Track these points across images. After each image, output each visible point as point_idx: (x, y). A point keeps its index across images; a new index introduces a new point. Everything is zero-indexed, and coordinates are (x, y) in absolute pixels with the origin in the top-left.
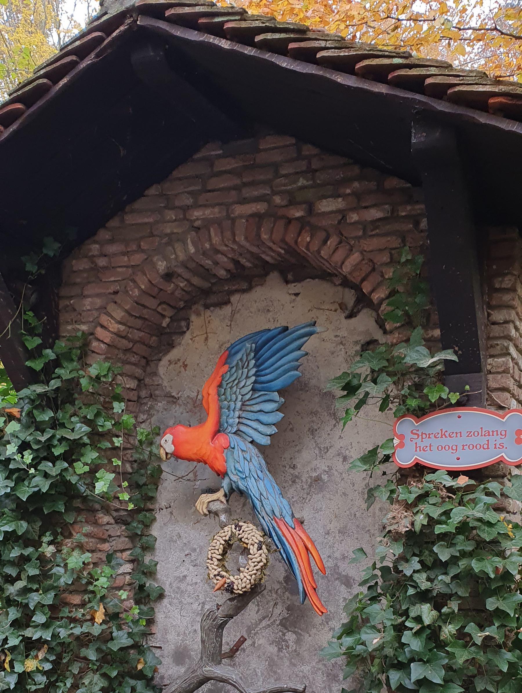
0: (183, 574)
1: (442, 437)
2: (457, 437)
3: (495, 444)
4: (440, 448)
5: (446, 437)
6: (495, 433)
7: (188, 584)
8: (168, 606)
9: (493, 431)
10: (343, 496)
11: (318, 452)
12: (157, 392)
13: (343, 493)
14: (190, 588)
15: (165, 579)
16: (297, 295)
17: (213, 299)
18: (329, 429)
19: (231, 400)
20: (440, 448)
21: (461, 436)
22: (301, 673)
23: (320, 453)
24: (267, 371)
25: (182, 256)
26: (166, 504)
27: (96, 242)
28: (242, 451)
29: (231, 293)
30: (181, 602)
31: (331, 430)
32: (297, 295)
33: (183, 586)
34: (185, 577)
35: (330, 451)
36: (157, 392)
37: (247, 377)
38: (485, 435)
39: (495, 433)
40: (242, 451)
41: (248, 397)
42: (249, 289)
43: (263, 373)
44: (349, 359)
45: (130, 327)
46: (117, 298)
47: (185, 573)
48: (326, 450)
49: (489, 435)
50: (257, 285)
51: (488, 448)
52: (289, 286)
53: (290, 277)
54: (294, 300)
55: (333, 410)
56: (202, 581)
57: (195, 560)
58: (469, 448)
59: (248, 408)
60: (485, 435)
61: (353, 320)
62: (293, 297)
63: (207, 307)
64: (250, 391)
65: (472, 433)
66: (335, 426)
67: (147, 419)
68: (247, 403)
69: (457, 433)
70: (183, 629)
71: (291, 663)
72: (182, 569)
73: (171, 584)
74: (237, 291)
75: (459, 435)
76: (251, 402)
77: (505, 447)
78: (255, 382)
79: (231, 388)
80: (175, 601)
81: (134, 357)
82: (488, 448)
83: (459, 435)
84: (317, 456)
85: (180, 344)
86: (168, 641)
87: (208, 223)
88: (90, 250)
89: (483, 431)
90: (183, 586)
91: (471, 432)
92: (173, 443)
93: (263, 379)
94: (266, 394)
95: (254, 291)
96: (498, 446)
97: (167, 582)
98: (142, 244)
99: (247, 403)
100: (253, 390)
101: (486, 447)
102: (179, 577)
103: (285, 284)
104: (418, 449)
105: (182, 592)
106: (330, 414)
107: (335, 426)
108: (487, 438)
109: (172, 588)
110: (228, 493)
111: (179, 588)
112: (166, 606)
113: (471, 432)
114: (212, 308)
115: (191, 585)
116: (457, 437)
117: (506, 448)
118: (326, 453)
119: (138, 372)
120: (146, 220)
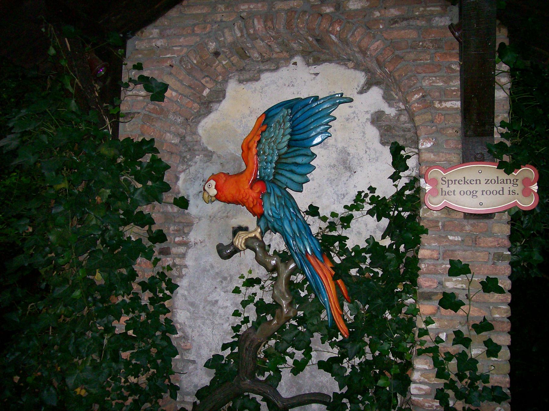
0: (215, 299)
1: (465, 184)
2: (476, 183)
3: (509, 191)
4: (462, 193)
5: (468, 184)
6: (509, 181)
7: (219, 308)
8: (202, 325)
9: (507, 180)
10: (358, 235)
11: (335, 198)
12: (196, 148)
13: (358, 232)
14: (221, 311)
15: (199, 303)
16: (317, 74)
17: (247, 76)
18: (345, 179)
19: (269, 154)
20: (462, 193)
21: (480, 183)
22: (320, 383)
23: (338, 198)
24: (301, 131)
25: (229, 39)
26: (200, 239)
27: (156, 27)
28: (278, 197)
29: (261, 71)
30: (213, 323)
31: (347, 180)
32: (317, 74)
33: (215, 309)
34: (217, 301)
35: (346, 197)
36: (196, 148)
37: (284, 135)
38: (501, 183)
39: (509, 181)
40: (278, 197)
41: (283, 151)
42: (277, 69)
43: (297, 133)
44: (361, 125)
45: (180, 94)
46: (173, 70)
47: (217, 298)
48: (343, 197)
49: (504, 183)
50: (282, 67)
51: (503, 194)
52: (310, 67)
53: (311, 61)
54: (314, 78)
55: (348, 164)
56: (232, 305)
57: (226, 287)
58: (487, 194)
59: (284, 161)
60: (501, 183)
61: (364, 95)
62: (314, 76)
63: (240, 82)
64: (286, 146)
65: (489, 181)
66: (350, 177)
67: (186, 169)
68: (284, 156)
69: (476, 180)
70: (215, 346)
71: (312, 375)
72: (214, 294)
73: (204, 307)
74: (267, 70)
75: (478, 182)
76: (287, 156)
77: (516, 194)
78: (290, 140)
79: (270, 143)
80: (208, 321)
81: (180, 118)
82: (503, 194)
83: (478, 182)
84: (335, 201)
85: (217, 110)
86: (201, 356)
87: (252, 15)
88: (152, 34)
89: (499, 180)
90: (215, 309)
91: (489, 180)
92: (216, 187)
93: (297, 137)
94: (299, 150)
95: (281, 70)
96: (511, 193)
97: (201, 306)
98: (196, 29)
99: (284, 156)
100: (289, 146)
101: (501, 192)
102: (211, 301)
103: (307, 66)
104: (444, 193)
105: (214, 314)
106: (346, 167)
107: (350, 177)
108: (503, 185)
109: (205, 310)
110: (264, 231)
111: (211, 311)
112: (199, 326)
113: (489, 180)
114: (245, 83)
115: (222, 308)
116: (476, 183)
117: (518, 194)
118: (342, 199)
119: (182, 131)
120: (199, 12)
